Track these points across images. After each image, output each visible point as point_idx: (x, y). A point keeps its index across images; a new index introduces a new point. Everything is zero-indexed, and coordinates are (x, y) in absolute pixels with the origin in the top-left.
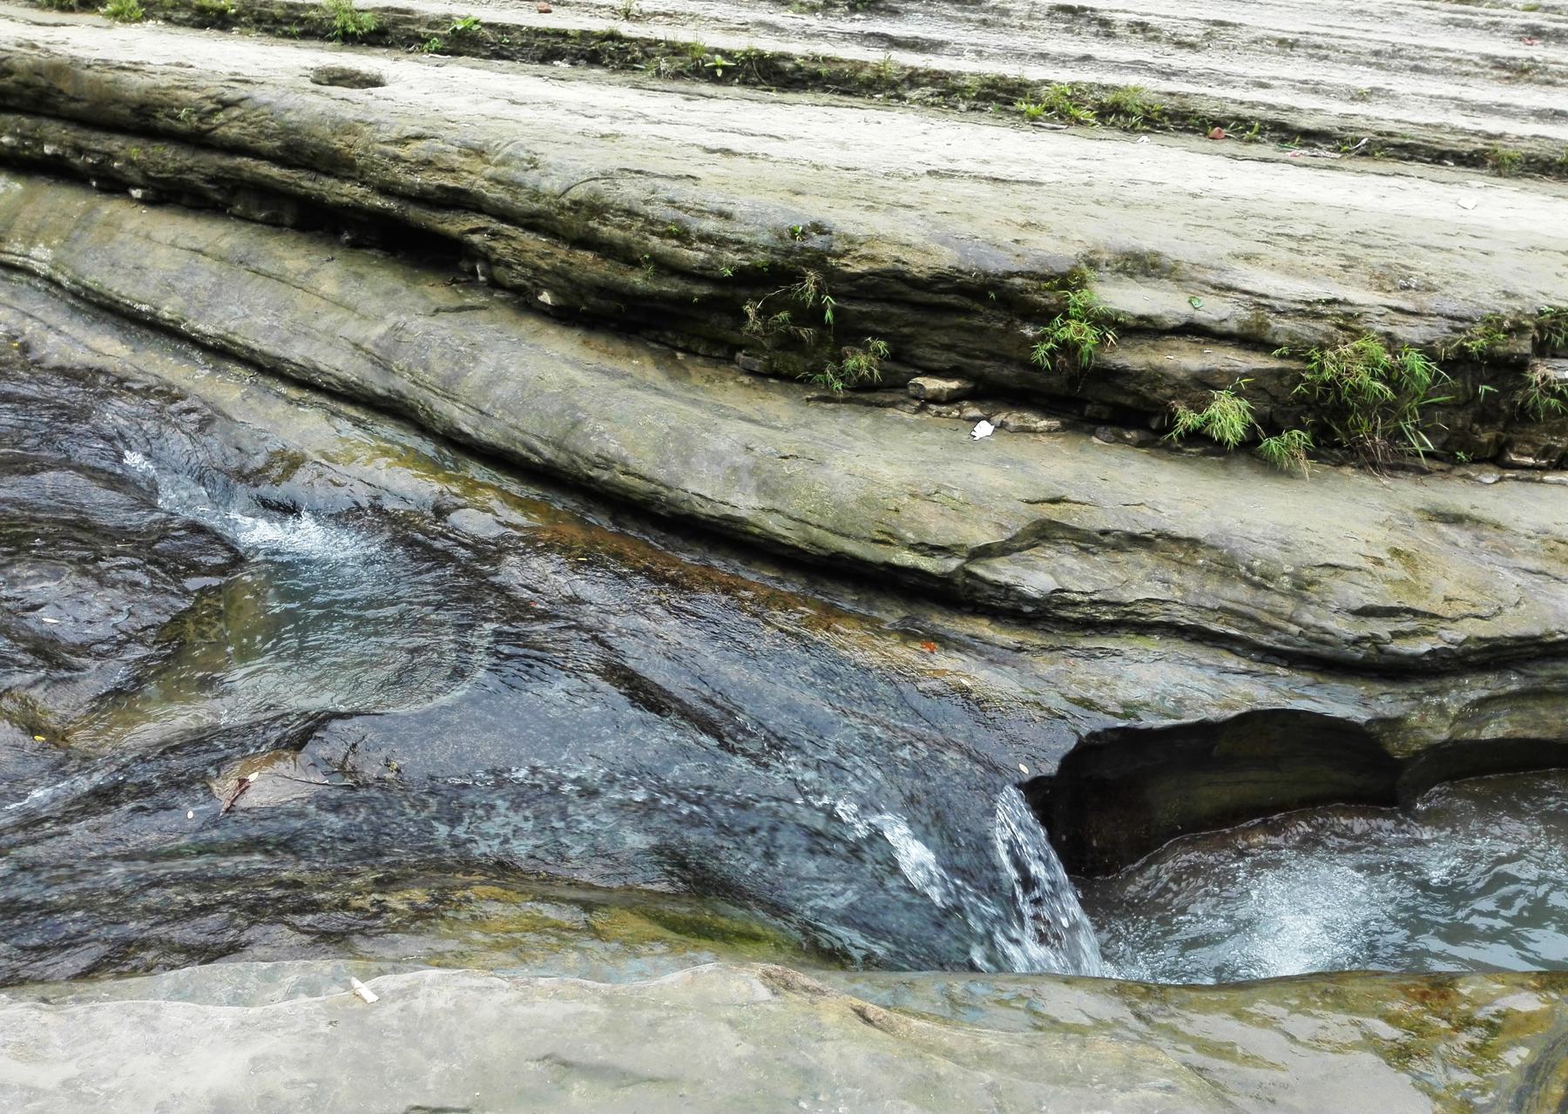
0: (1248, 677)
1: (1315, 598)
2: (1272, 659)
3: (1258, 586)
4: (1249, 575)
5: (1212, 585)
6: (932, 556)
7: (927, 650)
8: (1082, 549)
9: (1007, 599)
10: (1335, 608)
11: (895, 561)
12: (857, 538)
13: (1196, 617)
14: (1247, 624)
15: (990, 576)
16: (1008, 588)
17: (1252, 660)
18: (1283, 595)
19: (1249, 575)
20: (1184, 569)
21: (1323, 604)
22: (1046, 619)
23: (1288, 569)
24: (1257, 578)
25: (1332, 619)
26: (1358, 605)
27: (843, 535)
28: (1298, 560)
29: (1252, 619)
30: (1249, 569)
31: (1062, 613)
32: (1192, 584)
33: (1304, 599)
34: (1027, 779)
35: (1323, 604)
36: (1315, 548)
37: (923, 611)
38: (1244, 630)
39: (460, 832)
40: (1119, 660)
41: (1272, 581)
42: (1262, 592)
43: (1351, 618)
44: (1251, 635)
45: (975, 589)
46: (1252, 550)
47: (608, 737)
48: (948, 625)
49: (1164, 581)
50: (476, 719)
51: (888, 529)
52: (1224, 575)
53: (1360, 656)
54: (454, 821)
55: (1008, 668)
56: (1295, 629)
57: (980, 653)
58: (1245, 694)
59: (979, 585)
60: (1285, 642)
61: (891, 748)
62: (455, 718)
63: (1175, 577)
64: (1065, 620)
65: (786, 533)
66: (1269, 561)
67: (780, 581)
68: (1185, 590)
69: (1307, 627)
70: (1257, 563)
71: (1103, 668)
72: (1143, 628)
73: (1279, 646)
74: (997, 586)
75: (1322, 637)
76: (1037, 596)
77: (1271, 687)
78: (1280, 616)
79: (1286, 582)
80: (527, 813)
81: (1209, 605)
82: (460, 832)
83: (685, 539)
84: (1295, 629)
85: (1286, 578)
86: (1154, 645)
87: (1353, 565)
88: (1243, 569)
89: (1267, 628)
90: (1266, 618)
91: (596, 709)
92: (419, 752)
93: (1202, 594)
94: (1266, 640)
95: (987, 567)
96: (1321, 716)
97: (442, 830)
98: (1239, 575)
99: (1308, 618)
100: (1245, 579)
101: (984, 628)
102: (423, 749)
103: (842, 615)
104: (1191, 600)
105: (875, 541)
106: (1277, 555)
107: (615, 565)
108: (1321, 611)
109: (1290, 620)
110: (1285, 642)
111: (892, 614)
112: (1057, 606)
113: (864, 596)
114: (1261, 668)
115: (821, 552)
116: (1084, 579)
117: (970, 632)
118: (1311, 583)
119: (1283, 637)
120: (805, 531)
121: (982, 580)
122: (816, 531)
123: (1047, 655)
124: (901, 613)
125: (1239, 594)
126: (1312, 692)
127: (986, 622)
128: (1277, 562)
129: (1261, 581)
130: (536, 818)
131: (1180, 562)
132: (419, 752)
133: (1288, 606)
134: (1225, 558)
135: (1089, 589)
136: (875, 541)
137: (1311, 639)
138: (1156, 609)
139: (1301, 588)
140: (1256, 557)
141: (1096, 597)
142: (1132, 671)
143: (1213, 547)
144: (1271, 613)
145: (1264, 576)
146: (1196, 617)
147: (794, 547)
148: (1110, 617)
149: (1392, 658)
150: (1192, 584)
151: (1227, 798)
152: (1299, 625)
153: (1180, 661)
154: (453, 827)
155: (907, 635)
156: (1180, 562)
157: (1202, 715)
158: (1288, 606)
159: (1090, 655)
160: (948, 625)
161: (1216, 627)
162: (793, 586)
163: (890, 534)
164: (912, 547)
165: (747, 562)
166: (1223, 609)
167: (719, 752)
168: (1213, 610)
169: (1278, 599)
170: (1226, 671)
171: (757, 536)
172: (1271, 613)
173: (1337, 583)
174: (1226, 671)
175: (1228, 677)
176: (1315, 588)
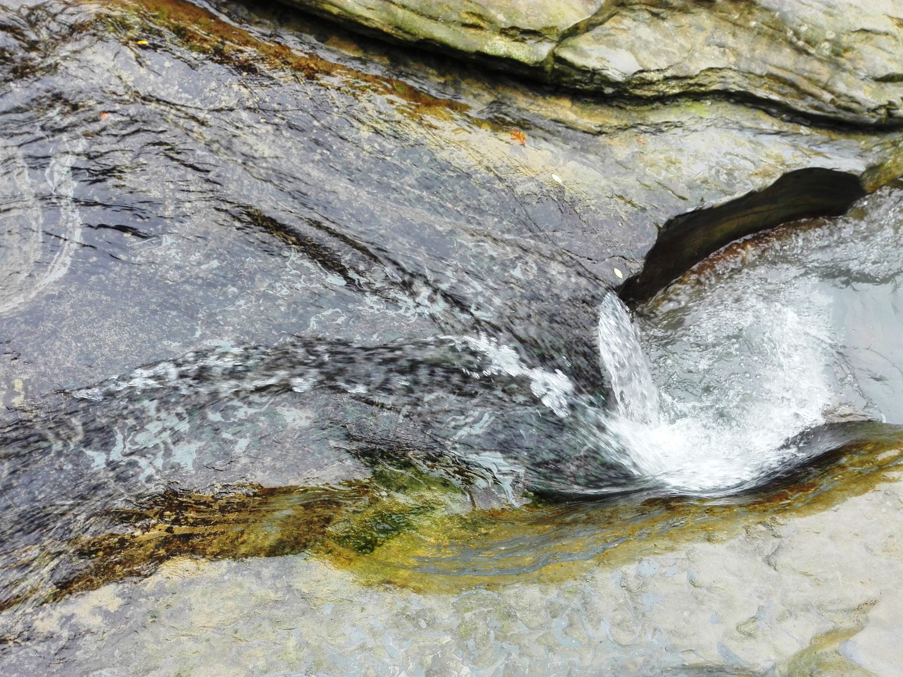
0: (777, 138)
1: (849, 65)
2: (799, 119)
3: (800, 51)
4: (794, 39)
5: (761, 49)
6: (523, 41)
7: (517, 142)
8: (654, 14)
9: (592, 81)
10: (863, 74)
11: (487, 50)
12: (447, 22)
13: (745, 83)
14: (788, 90)
15: (579, 61)
16: (594, 72)
17: (782, 120)
18: (820, 60)
19: (794, 39)
20: (738, 31)
21: (854, 72)
22: (624, 97)
23: (831, 35)
24: (801, 43)
25: (861, 88)
26: (882, 73)
27: (430, 17)
28: (839, 25)
29: (792, 85)
30: (796, 33)
31: (638, 92)
32: (744, 49)
33: (839, 67)
34: (621, 282)
35: (854, 72)
36: (854, 11)
37: (509, 93)
38: (784, 95)
39: (116, 454)
40: (679, 131)
41: (813, 46)
42: (803, 57)
43: (874, 85)
44: (788, 101)
45: (563, 74)
46: (801, 13)
47: (236, 297)
48: (534, 109)
49: (721, 46)
50: (90, 303)
51: (477, 10)
52: (772, 37)
53: (874, 121)
54: (106, 446)
55: (592, 157)
56: (827, 97)
57: (566, 140)
58: (777, 157)
59: (567, 70)
60: (816, 108)
61: (504, 266)
62: (66, 307)
63: (730, 41)
64: (639, 98)
65: (367, 14)
66: (815, 26)
67: (364, 62)
68: (738, 55)
69: (839, 96)
70: (804, 29)
71: (667, 143)
72: (695, 94)
73: (811, 111)
74: (583, 71)
75: (849, 105)
76: (620, 79)
77: (795, 147)
78: (816, 83)
79: (826, 48)
80: (180, 409)
81: (758, 72)
82: (116, 454)
83: (250, 8)
84: (827, 97)
85: (827, 45)
86: (706, 110)
87: (882, 28)
88: (790, 34)
89: (803, 94)
90: (805, 85)
91: (215, 263)
92: (41, 360)
93: (752, 59)
94: (801, 105)
95: (574, 49)
96: (830, 171)
97: (98, 459)
98: (786, 40)
99: (841, 87)
100: (791, 43)
101: (564, 110)
102: (43, 354)
103: (431, 103)
104: (743, 66)
105: (465, 25)
106: (822, 20)
107: (182, 51)
108: (852, 79)
109: (825, 88)
110: (816, 108)
111: (478, 99)
112: (635, 87)
113: (449, 78)
114: (787, 127)
115: (408, 37)
116: (657, 54)
117: (554, 116)
118: (846, 50)
119: (816, 103)
120: (390, 13)
121: (571, 65)
122: (400, 12)
123: (622, 135)
124: (488, 98)
125: (783, 60)
126: (825, 149)
127: (566, 103)
128: (821, 27)
129: (802, 48)
130: (190, 413)
131: (735, 24)
132: (41, 360)
133: (824, 72)
134: (776, 22)
135: (663, 65)
136: (465, 25)
137: (839, 107)
138: (714, 77)
139: (838, 54)
140: (804, 21)
141: (669, 73)
142: (693, 142)
143: (767, 10)
144: (810, 80)
145: (808, 42)
146: (745, 83)
147: (377, 30)
148: (677, 91)
149: (897, 120)
150: (744, 49)
151: (734, 226)
152: (832, 93)
153: (727, 126)
154: (108, 452)
155: (498, 124)
156: (735, 24)
157: (750, 188)
158: (824, 72)
159: (657, 129)
160: (534, 109)
161: (761, 93)
162: (377, 68)
163: (480, 16)
164: (503, 32)
165: (323, 38)
166: (770, 76)
167: (349, 293)
168: (761, 77)
169: (816, 65)
170: (762, 132)
171: (337, 16)
172: (810, 80)
173: (866, 49)
174: (762, 132)
175: (764, 139)
176: (848, 55)
